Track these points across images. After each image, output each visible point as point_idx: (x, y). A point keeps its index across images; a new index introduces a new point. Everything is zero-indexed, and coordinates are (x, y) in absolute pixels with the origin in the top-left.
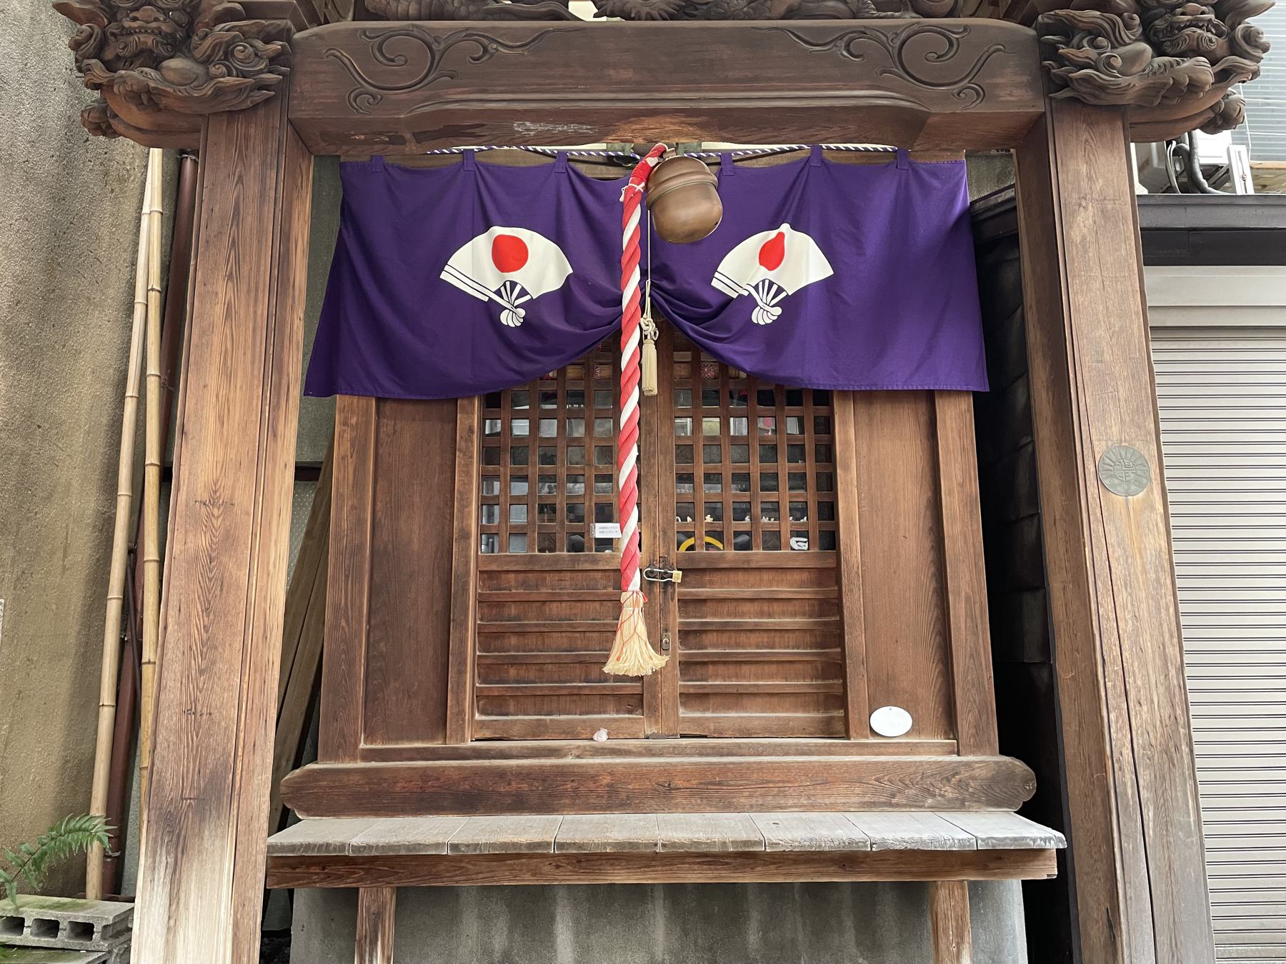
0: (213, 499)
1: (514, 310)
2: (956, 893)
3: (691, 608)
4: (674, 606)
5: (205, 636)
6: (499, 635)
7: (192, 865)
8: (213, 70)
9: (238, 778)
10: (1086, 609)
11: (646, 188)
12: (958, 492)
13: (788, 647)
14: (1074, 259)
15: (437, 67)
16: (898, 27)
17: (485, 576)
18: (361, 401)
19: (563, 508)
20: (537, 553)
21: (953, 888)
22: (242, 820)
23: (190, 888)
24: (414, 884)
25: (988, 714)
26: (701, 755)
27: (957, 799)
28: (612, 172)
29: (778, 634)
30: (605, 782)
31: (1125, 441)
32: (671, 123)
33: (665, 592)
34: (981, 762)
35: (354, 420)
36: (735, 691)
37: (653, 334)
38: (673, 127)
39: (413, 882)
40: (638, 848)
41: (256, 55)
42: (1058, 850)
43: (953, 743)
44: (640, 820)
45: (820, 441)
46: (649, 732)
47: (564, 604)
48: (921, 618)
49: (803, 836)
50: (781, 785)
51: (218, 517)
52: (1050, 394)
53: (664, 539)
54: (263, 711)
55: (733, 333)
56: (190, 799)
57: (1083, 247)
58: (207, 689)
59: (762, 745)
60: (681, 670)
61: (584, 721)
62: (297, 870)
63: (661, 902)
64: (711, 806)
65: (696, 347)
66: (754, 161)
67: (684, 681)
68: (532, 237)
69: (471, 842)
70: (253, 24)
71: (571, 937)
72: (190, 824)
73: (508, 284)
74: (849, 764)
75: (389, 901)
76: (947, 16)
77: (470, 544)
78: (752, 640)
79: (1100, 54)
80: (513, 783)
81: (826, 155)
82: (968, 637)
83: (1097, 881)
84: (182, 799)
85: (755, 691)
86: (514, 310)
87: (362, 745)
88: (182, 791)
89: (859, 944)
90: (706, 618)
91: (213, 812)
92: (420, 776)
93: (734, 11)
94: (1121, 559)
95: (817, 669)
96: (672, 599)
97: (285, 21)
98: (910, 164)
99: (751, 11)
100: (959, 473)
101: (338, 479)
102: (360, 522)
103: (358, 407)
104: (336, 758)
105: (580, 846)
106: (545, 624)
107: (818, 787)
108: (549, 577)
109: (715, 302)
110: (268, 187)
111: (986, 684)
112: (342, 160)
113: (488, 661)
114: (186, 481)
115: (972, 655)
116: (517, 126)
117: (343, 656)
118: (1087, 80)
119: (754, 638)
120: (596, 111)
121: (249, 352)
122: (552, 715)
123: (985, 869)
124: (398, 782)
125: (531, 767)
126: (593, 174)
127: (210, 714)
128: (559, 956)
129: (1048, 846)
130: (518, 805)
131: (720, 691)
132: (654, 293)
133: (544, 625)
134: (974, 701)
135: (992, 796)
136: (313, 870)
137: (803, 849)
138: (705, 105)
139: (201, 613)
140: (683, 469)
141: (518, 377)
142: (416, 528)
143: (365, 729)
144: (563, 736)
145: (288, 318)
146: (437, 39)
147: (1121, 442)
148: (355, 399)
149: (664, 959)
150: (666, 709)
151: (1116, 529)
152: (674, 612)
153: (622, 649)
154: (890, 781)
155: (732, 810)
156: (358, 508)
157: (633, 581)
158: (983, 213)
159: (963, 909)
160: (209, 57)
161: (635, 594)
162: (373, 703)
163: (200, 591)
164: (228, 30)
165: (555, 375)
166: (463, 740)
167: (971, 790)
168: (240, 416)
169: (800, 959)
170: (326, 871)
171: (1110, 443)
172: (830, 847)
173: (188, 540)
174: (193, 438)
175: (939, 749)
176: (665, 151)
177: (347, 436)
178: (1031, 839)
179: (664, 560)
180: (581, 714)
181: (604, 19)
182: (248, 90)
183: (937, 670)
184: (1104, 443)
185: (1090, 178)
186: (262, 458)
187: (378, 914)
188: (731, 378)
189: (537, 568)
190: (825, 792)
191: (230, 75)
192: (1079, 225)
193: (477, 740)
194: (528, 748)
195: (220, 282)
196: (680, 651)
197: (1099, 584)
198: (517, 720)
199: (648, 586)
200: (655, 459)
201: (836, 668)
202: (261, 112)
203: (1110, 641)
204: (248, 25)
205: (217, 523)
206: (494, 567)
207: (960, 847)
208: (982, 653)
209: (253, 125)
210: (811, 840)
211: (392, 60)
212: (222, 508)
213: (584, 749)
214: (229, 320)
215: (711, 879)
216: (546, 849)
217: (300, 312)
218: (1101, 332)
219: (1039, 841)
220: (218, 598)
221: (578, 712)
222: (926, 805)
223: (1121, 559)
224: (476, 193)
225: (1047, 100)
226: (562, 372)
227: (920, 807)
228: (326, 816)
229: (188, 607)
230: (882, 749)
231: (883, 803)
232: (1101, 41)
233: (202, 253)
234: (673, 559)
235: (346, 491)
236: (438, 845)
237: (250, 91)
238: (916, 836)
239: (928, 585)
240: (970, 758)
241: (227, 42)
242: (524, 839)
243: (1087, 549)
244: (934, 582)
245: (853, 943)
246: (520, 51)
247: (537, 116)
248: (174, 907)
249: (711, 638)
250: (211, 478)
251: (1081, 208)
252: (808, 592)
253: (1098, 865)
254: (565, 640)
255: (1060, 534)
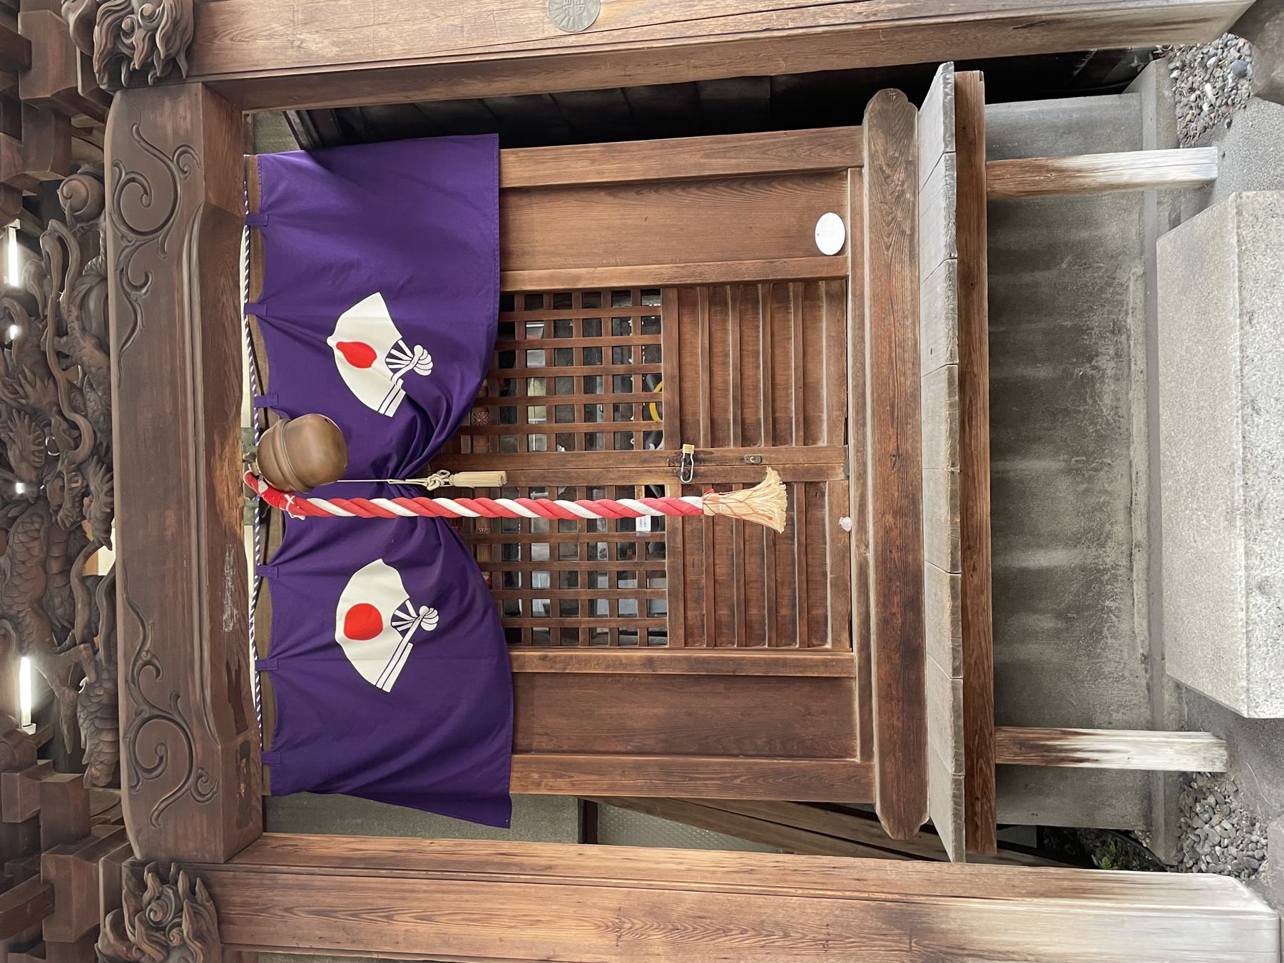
0: (614, 929)
1: (421, 617)
2: (998, 172)
3: (720, 434)
4: (718, 451)
5: (750, 933)
6: (748, 625)
7: (974, 940)
8: (176, 942)
9: (890, 896)
10: (715, 47)
11: (290, 493)
12: (600, 165)
13: (758, 337)
14: (356, 55)
15: (169, 713)
16: (115, 235)
17: (690, 640)
18: (515, 769)
19: (623, 564)
20: (665, 532)
21: (994, 176)
22: (931, 891)
23: (997, 941)
24: (992, 710)
25: (822, 137)
26: (864, 425)
27: (906, 168)
28: (276, 520)
29: (745, 347)
30: (891, 520)
31: (544, 4)
32: (222, 469)
33: (704, 461)
34: (869, 143)
35: (535, 776)
36: (802, 390)
37: (443, 476)
38: (226, 467)
39: (990, 712)
40: (956, 490)
41: (159, 898)
42: (955, 71)
43: (851, 172)
44: (929, 486)
45: (550, 304)
46: (842, 476)
47: (717, 562)
48: (729, 202)
49: (944, 326)
50: (893, 345)
51: (633, 924)
52: (496, 79)
53: (652, 462)
54: (826, 872)
55: (443, 396)
56: (911, 943)
57: (344, 44)
58: (802, 929)
59: (854, 363)
60: (782, 444)
61: (832, 540)
62: (979, 824)
63: (1008, 463)
64: (914, 415)
65: (458, 430)
66: (262, 373)
67: (792, 441)
68: (345, 600)
69: (951, 656)
70: (126, 903)
71: (1042, 551)
72: (935, 943)
73: (394, 624)
74: (872, 277)
75: (1008, 734)
76: (103, 184)
77: (658, 657)
78: (750, 374)
79: (140, 26)
80: (893, 610)
81: (254, 299)
82: (746, 156)
83: (987, 38)
84: (911, 951)
85: (801, 370)
86: (421, 617)
87: (857, 760)
88: (902, 951)
89: (1048, 267)
90: (729, 419)
91: (924, 919)
92: (887, 702)
93: (103, 406)
94: (665, 10)
95: (779, 307)
96: (711, 453)
97: (123, 868)
98: (262, 212)
99: (101, 387)
100: (580, 164)
101: (594, 790)
102: (638, 767)
103: (522, 772)
104: (870, 785)
105: (954, 547)
106: (737, 581)
107: (895, 307)
108: (690, 577)
109: (410, 413)
110: (297, 882)
111: (792, 138)
112: (268, 793)
113: (774, 635)
114: (598, 956)
115: (764, 152)
116: (228, 628)
117: (770, 781)
118: (167, 39)
119: (748, 372)
120: (211, 549)
121: (466, 897)
122: (826, 572)
123: (975, 144)
124: (893, 724)
125: (878, 593)
126: (279, 538)
127: (828, 925)
128: (1060, 563)
129: (952, 81)
130: (914, 605)
131: (801, 405)
132: (402, 476)
133: (738, 581)
134: (809, 150)
135: (903, 133)
136: (978, 808)
137: (956, 327)
138: (202, 436)
139: (728, 938)
140: (581, 443)
141: (490, 611)
142: (643, 711)
143: (841, 757)
144: (847, 561)
145: (429, 856)
146: (138, 712)
147: (545, 8)
148: (514, 775)
149: (1064, 460)
150: (820, 459)
151: (634, 15)
152: (724, 451)
153: (759, 514)
154: (889, 236)
155: (918, 446)
156: (624, 770)
157: (693, 503)
158: (311, 137)
159: (1014, 166)
160: (162, 946)
161: (706, 502)
162: (816, 749)
163: (705, 939)
164: (134, 927)
165: (486, 573)
166: (852, 660)
167: (897, 155)
168: (531, 904)
169: (1062, 326)
170: (979, 796)
171: (546, 20)
172: (954, 300)
173: (656, 952)
174: (554, 951)
175: (857, 186)
176: (251, 473)
177: (551, 782)
178: (945, 98)
179: (671, 463)
180: (825, 543)
181: (113, 538)
182: (195, 905)
183: (778, 187)
184: (546, 26)
185: (270, 37)
186: (573, 880)
187: (1020, 744)
188: (487, 395)
189: (682, 589)
190: (900, 301)
191: (180, 925)
192: (320, 49)
193: (851, 646)
194: (859, 597)
195: (395, 928)
196: (763, 445)
197: (690, 33)
198: (832, 607)
199: (699, 478)
200: (570, 472)
201: (778, 289)
202: (217, 890)
203: (746, 23)
204: (128, 907)
205: (638, 924)
206: (681, 632)
207: (953, 170)
208: (761, 142)
209: (233, 898)
210: (947, 318)
211: (161, 758)
212: (623, 919)
213: (859, 541)
214: (433, 918)
215: (985, 417)
216: (957, 581)
217: (425, 844)
218: (432, 27)
219: (947, 90)
220: (713, 921)
221: (823, 546)
222: (912, 199)
223: (665, 10)
224: (302, 657)
225: (189, 80)
226: (483, 567)
227: (914, 205)
228: (926, 793)
229: (722, 950)
230: (858, 243)
231: (910, 242)
232: (127, 24)
233: (365, 947)
234: (671, 453)
235: (606, 781)
236: (954, 688)
237: (197, 903)
238: (943, 213)
239: (693, 196)
240: (866, 154)
241: (146, 929)
242: (948, 604)
243: (655, 45)
244: (691, 189)
245: (1047, 274)
246: (148, 628)
247: (216, 608)
248: (1015, 956)
249: (748, 413)
250: (594, 932)
251: (303, 46)
252: (703, 316)
253: (971, 36)
254: (753, 560)
255: (640, 71)
